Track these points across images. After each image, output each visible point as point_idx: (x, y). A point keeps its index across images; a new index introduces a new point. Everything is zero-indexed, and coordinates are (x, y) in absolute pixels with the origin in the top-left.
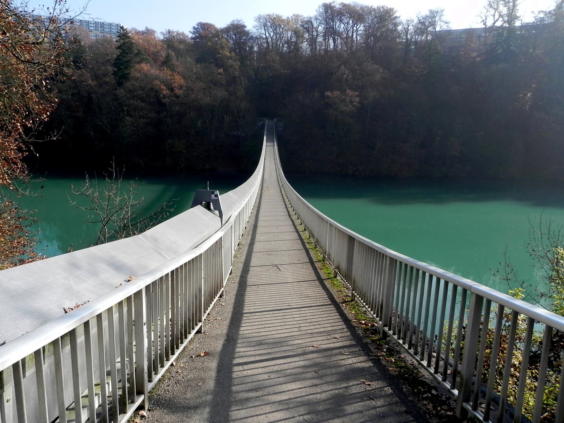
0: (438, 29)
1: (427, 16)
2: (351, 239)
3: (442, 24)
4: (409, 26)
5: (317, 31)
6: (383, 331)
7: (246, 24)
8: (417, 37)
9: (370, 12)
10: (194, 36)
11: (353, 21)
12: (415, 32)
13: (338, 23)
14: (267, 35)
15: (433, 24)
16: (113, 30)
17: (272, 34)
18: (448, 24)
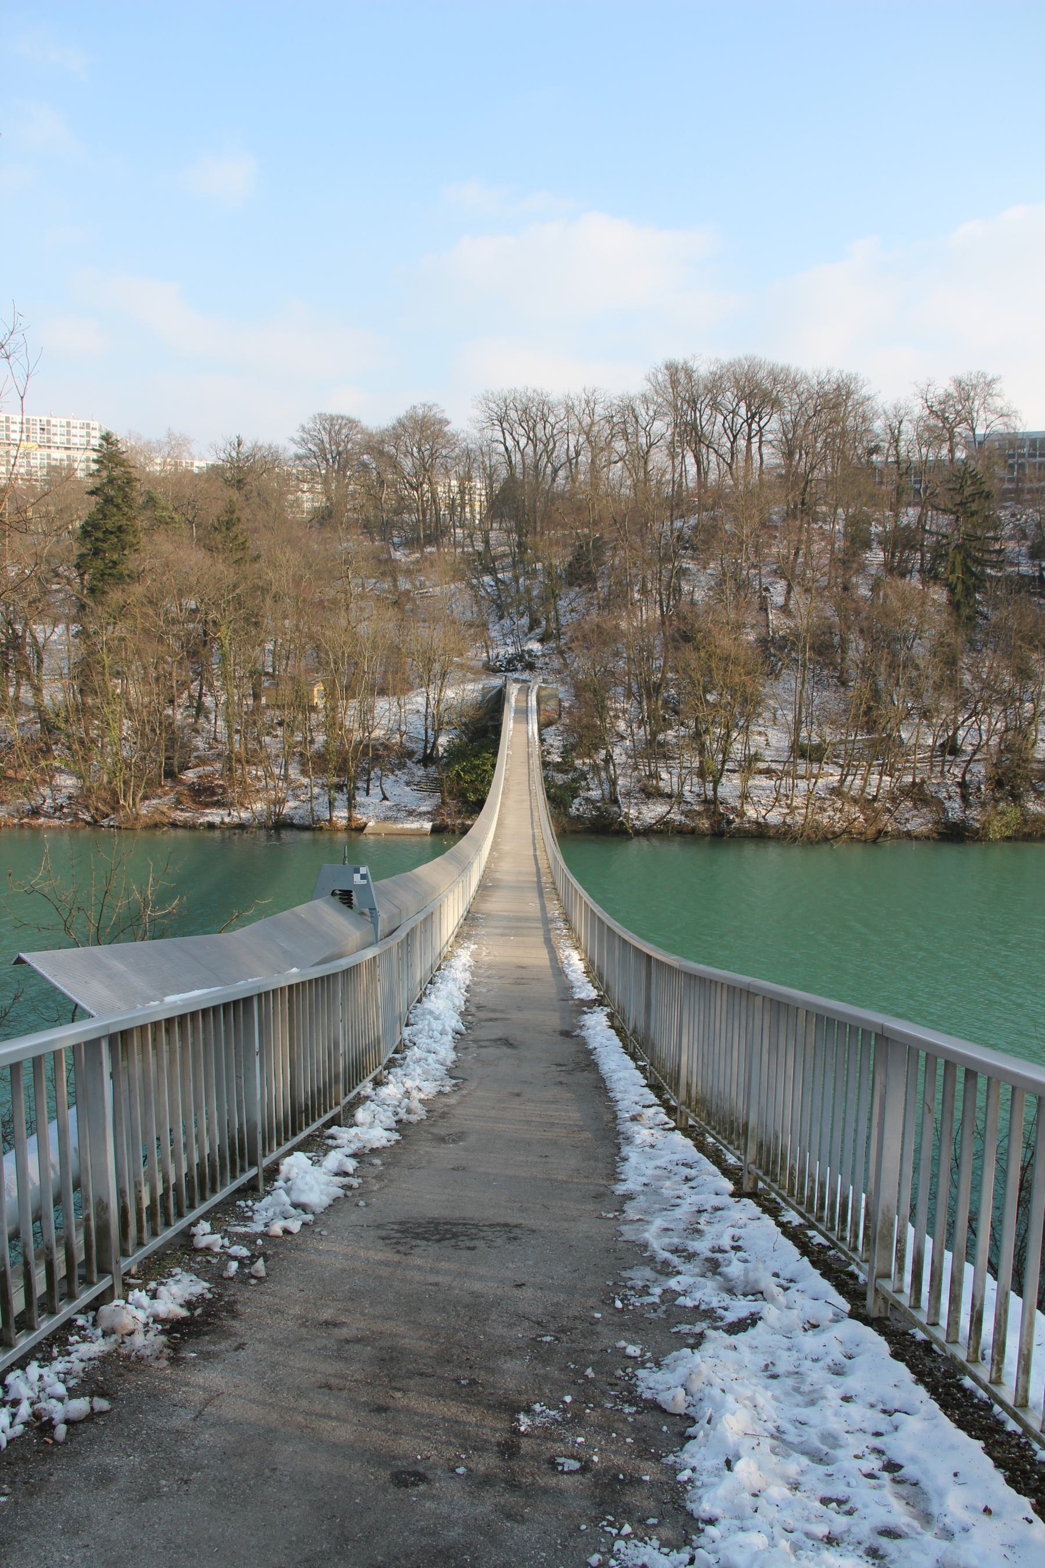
0: (980, 431)
1: (949, 396)
2: (649, 957)
3: (991, 417)
4: (900, 423)
5: (649, 435)
6: (309, 777)
7: (447, 416)
8: (924, 450)
9: (796, 385)
10: (302, 452)
11: (748, 409)
12: (919, 437)
13: (708, 411)
14: (510, 443)
15: (968, 419)
16: (74, 440)
17: (523, 441)
18: (1006, 419)
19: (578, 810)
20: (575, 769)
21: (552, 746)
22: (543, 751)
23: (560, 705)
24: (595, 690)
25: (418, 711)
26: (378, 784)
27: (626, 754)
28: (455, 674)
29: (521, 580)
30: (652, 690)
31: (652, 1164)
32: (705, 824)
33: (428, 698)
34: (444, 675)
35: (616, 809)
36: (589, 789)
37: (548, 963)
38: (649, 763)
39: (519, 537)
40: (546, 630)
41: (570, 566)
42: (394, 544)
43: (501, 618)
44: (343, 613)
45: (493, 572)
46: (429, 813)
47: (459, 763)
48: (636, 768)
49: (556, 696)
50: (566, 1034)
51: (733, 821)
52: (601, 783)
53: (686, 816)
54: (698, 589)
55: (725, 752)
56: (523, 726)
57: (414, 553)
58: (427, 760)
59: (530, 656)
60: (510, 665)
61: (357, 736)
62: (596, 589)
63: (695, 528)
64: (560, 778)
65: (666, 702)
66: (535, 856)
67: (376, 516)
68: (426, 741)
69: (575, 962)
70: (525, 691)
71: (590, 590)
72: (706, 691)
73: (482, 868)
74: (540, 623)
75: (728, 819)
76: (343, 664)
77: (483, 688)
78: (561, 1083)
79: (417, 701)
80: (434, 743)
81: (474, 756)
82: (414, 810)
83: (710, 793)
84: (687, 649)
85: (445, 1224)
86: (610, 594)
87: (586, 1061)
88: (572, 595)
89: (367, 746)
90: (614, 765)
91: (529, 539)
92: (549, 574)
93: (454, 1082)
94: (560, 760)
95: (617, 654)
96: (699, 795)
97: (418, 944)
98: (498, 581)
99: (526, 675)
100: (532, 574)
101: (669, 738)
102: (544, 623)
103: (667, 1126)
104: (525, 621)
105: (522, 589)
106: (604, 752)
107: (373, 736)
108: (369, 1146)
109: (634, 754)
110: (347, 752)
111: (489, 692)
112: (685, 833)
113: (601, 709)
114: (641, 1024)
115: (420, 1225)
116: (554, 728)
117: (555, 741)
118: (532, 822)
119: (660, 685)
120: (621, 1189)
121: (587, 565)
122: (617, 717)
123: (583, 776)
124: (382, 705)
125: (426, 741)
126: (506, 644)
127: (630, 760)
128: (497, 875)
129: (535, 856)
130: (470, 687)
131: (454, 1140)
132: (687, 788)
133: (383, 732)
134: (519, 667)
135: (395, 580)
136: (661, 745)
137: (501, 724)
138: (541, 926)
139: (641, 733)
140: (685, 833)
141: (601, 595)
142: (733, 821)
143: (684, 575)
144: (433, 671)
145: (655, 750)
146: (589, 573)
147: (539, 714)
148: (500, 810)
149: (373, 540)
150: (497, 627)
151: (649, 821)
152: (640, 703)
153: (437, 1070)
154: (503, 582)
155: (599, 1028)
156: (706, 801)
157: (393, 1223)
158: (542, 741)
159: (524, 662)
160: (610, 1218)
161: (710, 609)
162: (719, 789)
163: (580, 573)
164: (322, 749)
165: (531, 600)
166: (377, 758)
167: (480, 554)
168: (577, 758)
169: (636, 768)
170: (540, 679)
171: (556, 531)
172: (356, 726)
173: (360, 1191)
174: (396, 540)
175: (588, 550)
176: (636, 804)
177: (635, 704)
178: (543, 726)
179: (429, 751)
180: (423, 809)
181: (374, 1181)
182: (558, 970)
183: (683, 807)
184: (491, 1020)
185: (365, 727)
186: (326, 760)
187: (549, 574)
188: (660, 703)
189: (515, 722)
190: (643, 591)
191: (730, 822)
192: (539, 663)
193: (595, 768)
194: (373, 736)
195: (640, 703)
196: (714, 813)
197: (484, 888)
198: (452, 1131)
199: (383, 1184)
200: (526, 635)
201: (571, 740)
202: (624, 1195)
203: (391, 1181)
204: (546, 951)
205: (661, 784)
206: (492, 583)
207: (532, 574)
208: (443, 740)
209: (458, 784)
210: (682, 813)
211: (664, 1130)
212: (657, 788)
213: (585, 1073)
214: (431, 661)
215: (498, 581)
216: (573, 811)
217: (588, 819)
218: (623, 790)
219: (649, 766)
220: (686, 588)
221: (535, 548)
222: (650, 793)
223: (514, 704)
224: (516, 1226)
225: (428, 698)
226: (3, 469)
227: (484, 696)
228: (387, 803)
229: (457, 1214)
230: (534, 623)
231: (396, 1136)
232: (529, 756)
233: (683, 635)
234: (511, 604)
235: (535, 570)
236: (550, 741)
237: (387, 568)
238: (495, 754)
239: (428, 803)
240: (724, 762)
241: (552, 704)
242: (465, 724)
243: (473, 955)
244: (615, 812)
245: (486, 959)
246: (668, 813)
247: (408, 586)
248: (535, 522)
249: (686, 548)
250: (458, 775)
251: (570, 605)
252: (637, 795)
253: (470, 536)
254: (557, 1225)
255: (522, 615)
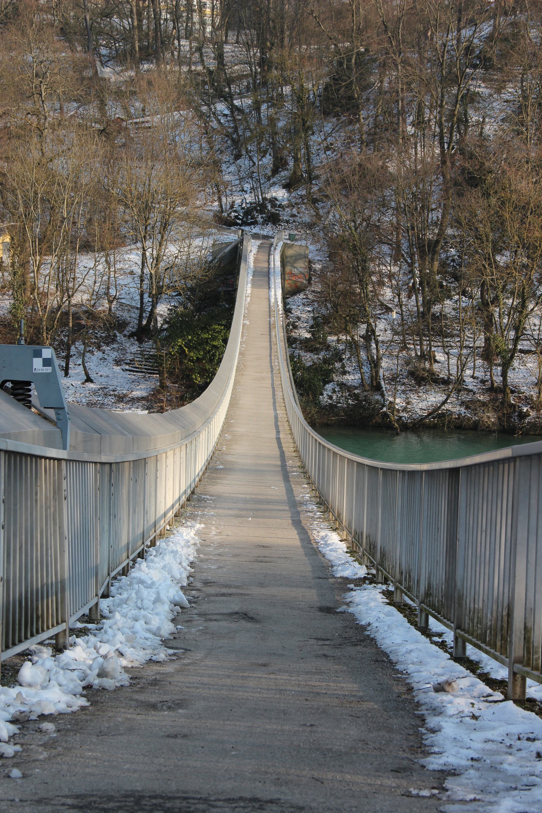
19: (331, 398)
20: (328, 347)
21: (299, 318)
22: (288, 325)
23: (310, 268)
24: (354, 246)
25: (132, 273)
26: (80, 361)
27: (392, 329)
28: (177, 229)
29: (264, 107)
30: (428, 249)
31: (479, 736)
32: (490, 417)
33: (144, 255)
34: (165, 226)
35: (378, 397)
36: (344, 373)
37: (298, 543)
38: (421, 340)
39: (263, 53)
40: (295, 172)
41: (326, 89)
42: (100, 55)
43: (238, 157)
44: (35, 140)
45: (228, 98)
46: (143, 398)
47: (182, 336)
48: (404, 347)
49: (306, 256)
50: (328, 610)
51: (527, 415)
52: (360, 366)
53: (467, 408)
54: (490, 121)
55: (518, 328)
56: (263, 292)
57: (126, 70)
58: (142, 333)
59: (274, 206)
60: (248, 217)
61: (53, 302)
62: (358, 120)
63: (490, 38)
64: (308, 359)
65: (443, 264)
66: (278, 440)
67: (76, 17)
68: (142, 310)
69: (334, 544)
70: (267, 248)
71: (351, 122)
72: (497, 250)
73: (211, 448)
74: (286, 163)
75: (521, 412)
76: (36, 207)
77: (214, 245)
78: (325, 656)
79: (131, 258)
80: (152, 312)
81: (202, 329)
82: (125, 395)
83: (498, 380)
84: (473, 198)
85: (151, 797)
86: (376, 126)
87: (360, 636)
88: (328, 127)
89: (67, 314)
90: (377, 342)
91: (274, 55)
92: (300, 99)
93: (171, 651)
94: (308, 336)
95: (384, 204)
96: (483, 382)
97: (125, 491)
98: (233, 108)
99: (267, 230)
100: (276, 101)
101: (447, 310)
102: (291, 163)
103: (490, 699)
104: (268, 160)
105: (265, 122)
106: (365, 326)
107: (74, 301)
108: (38, 711)
109: (403, 330)
110: (41, 320)
111: (221, 249)
112: (465, 429)
113: (361, 273)
114: (440, 575)
115: (111, 798)
116: (302, 296)
117: (303, 312)
118: (274, 403)
119: (437, 242)
120: (434, 763)
121: (349, 87)
122: (381, 283)
123: (338, 356)
124: (85, 261)
125: (142, 310)
126: (243, 190)
127: (396, 338)
128: (229, 458)
129: (278, 440)
130: (197, 242)
131: (169, 708)
132: (468, 372)
133: (86, 297)
134: (260, 219)
135: (103, 104)
136: (436, 318)
137: (236, 290)
138: (287, 508)
139: (412, 304)
140: (465, 429)
141: (365, 128)
142: (527, 415)
143: (472, 101)
144: (149, 222)
145: (429, 326)
146: (351, 98)
147: (283, 279)
148: (234, 389)
149: (73, 50)
150: (232, 168)
151: (420, 413)
152: (411, 265)
153: (147, 639)
154: (240, 110)
155: (372, 604)
156: (492, 389)
157: (66, 797)
158: (287, 311)
159: (265, 214)
160: (424, 797)
161: (504, 143)
162: (510, 374)
163: (339, 101)
164: (10, 316)
165: (276, 133)
166: (78, 328)
167: (210, 72)
168: (330, 334)
169: (404, 347)
170: (285, 235)
171: (309, 45)
172: (53, 287)
173: (15, 760)
174: (104, 51)
175: (349, 68)
176: (404, 392)
177: (405, 267)
178: (287, 294)
179: (144, 322)
180: (137, 394)
181: (40, 749)
182: (313, 551)
183: (464, 397)
184: (223, 595)
185: (66, 292)
186: (14, 329)
187: (300, 99)
188: (436, 264)
189: (254, 286)
190: (419, 123)
191: (523, 416)
192: (285, 215)
193: (352, 346)
194: (74, 301)
195: (411, 265)
196: (502, 403)
197: (214, 468)
198: (165, 698)
199: (54, 752)
200: (269, 179)
201: (324, 311)
202: (442, 771)
203: (69, 749)
204: (295, 532)
205: (436, 367)
206: (227, 112)
207: (276, 101)
208: (162, 309)
209: (181, 363)
210: (462, 403)
211: (486, 701)
212: (431, 373)
213: (359, 648)
214: (148, 208)
215: (233, 108)
216: (324, 399)
217: (343, 409)
218: (387, 374)
219: (421, 345)
220: (474, 117)
221: (281, 67)
222: (421, 378)
223: (252, 264)
224: (271, 801)
225: (144, 255)
226: (27, 809)
227: (214, 254)
228: (90, 385)
229: (173, 787)
230: (279, 164)
231: (83, 702)
232: (271, 327)
233: (470, 176)
234: (250, 139)
235: (281, 95)
236: (296, 312)
237: (93, 89)
238: (228, 327)
239: (143, 386)
240: (516, 340)
241: (301, 266)
242: (192, 289)
243: (198, 533)
244: (377, 402)
245: (216, 537)
246: (444, 403)
247: (120, 114)
248: (282, 32)
249: (475, 67)
250: (182, 352)
251: (327, 144)
252: (406, 381)
253: (199, 49)
254: (339, 801)
255: (264, 153)
